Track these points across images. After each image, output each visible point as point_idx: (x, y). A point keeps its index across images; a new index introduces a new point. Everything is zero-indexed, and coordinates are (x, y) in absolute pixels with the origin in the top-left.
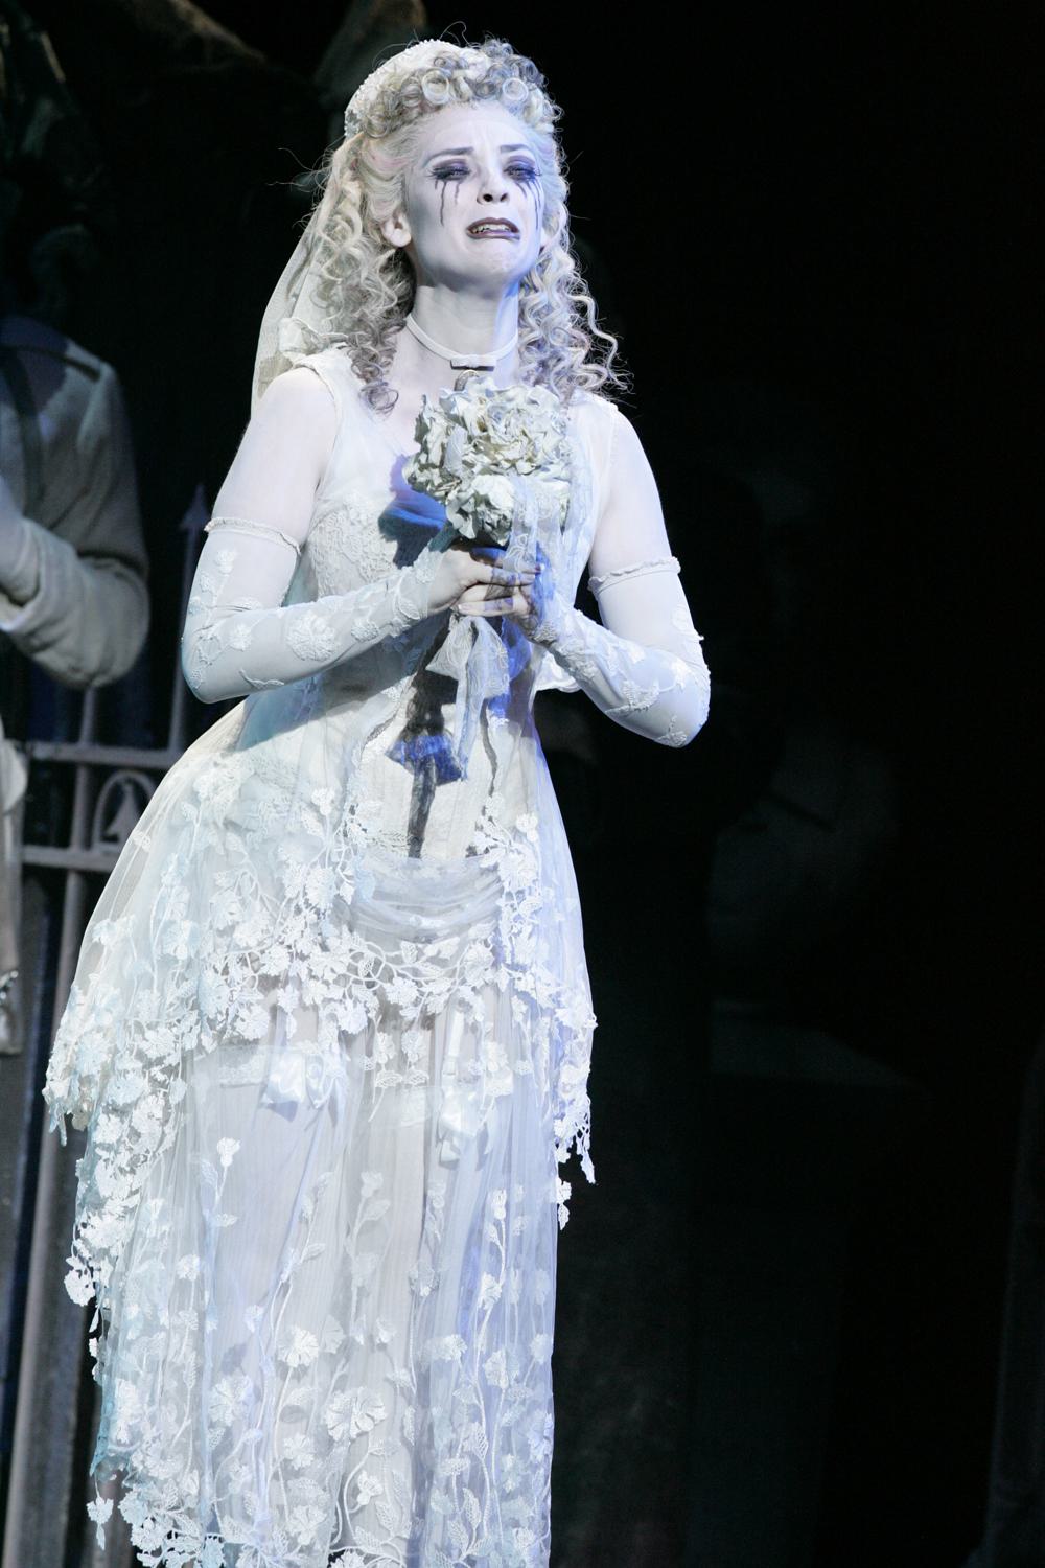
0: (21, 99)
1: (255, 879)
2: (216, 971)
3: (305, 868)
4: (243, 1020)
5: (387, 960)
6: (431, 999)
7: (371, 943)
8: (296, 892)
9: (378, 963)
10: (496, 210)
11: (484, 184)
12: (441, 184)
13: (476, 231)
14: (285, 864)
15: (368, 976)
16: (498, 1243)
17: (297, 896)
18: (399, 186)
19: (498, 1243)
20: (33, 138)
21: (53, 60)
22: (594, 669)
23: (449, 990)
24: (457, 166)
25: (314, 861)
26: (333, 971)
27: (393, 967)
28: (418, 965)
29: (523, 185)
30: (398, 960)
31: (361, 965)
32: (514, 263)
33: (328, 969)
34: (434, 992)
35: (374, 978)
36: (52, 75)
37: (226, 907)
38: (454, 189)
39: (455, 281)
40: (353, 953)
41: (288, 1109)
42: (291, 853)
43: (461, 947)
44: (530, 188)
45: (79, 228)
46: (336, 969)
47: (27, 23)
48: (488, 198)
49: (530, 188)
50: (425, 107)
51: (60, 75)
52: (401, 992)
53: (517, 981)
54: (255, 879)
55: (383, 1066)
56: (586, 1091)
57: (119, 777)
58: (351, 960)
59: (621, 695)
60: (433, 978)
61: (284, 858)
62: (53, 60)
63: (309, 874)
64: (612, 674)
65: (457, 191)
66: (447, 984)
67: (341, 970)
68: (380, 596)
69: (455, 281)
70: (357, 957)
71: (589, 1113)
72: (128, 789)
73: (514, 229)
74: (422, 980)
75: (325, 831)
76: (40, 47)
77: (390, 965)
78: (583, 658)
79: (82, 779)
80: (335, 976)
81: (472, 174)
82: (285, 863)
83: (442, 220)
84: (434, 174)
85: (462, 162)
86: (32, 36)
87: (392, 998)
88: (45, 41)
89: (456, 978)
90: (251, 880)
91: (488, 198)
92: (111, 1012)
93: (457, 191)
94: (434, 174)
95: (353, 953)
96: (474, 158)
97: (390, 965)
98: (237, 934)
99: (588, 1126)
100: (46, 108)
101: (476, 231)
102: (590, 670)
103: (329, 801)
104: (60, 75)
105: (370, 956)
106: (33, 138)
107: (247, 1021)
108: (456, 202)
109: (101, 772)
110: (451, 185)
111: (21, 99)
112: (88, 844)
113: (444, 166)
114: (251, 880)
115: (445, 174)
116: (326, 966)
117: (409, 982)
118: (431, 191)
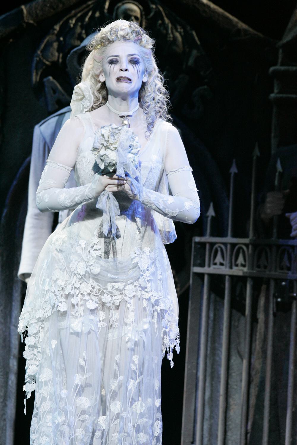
0: (187, 50)
1: (65, 266)
2: (52, 292)
3: (76, 263)
4: (60, 306)
5: (103, 289)
6: (115, 301)
7: (98, 284)
8: (74, 269)
9: (99, 290)
10: (124, 74)
11: (121, 66)
12: (110, 65)
13: (119, 79)
14: (72, 261)
15: (97, 293)
16: (136, 371)
17: (74, 270)
18: (102, 64)
19: (136, 371)
20: (191, 61)
21: (196, 38)
22: (155, 206)
23: (121, 298)
24: (115, 60)
25: (79, 260)
26: (86, 291)
27: (105, 291)
28: (112, 291)
29: (134, 65)
30: (107, 289)
31: (94, 290)
32: (129, 89)
33: (85, 291)
34: (116, 299)
35: (98, 294)
36: (197, 43)
37: (57, 274)
38: (113, 67)
39: (116, 95)
40: (92, 287)
41: (77, 334)
42: (74, 258)
43: (125, 286)
44: (136, 66)
45: (206, 87)
46: (87, 291)
47: (188, 28)
48: (122, 70)
49: (136, 66)
50: (110, 42)
51: (199, 43)
52: (106, 298)
53: (143, 295)
54: (65, 266)
55: (101, 321)
56: (178, 327)
57: (217, 246)
58: (91, 289)
59: (166, 213)
60: (116, 295)
61: (72, 259)
62: (196, 38)
63: (78, 264)
64: (161, 208)
65: (114, 68)
66: (120, 296)
67: (89, 291)
68: (91, 185)
69: (116, 95)
70: (93, 288)
71: (179, 333)
72: (219, 249)
73: (130, 80)
74: (113, 295)
75: (83, 253)
76: (192, 35)
77: (103, 290)
78: (151, 203)
79: (208, 247)
80: (87, 293)
81: (119, 62)
82: (72, 260)
83: (110, 76)
84: (109, 62)
85: (116, 59)
86: (190, 32)
87: (103, 300)
88: (194, 33)
89: (123, 295)
90: (64, 266)
91: (122, 70)
92: (30, 307)
93: (114, 68)
94: (109, 62)
95: (92, 287)
96: (120, 58)
97: (103, 290)
98: (58, 282)
99: (179, 337)
100: (195, 52)
101: (119, 79)
102: (153, 207)
103: (84, 244)
104: (199, 43)
105: (97, 287)
106: (191, 61)
107: (61, 306)
108: (113, 71)
109: (212, 244)
110: (113, 65)
111: (187, 50)
112: (209, 266)
113: (111, 60)
114: (64, 266)
115: (112, 62)
116: (84, 290)
117: (109, 296)
118: (108, 67)
